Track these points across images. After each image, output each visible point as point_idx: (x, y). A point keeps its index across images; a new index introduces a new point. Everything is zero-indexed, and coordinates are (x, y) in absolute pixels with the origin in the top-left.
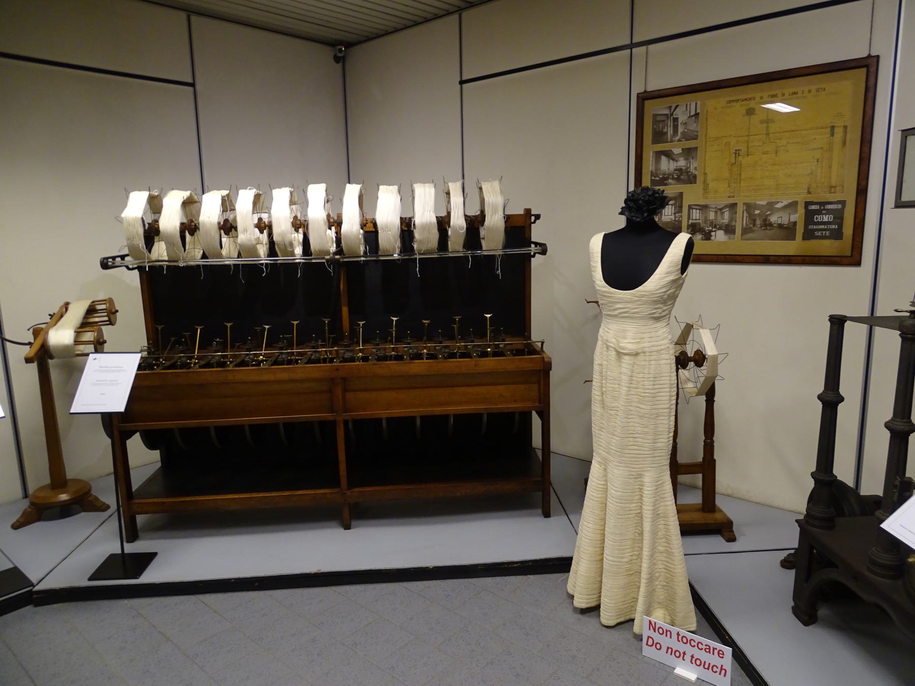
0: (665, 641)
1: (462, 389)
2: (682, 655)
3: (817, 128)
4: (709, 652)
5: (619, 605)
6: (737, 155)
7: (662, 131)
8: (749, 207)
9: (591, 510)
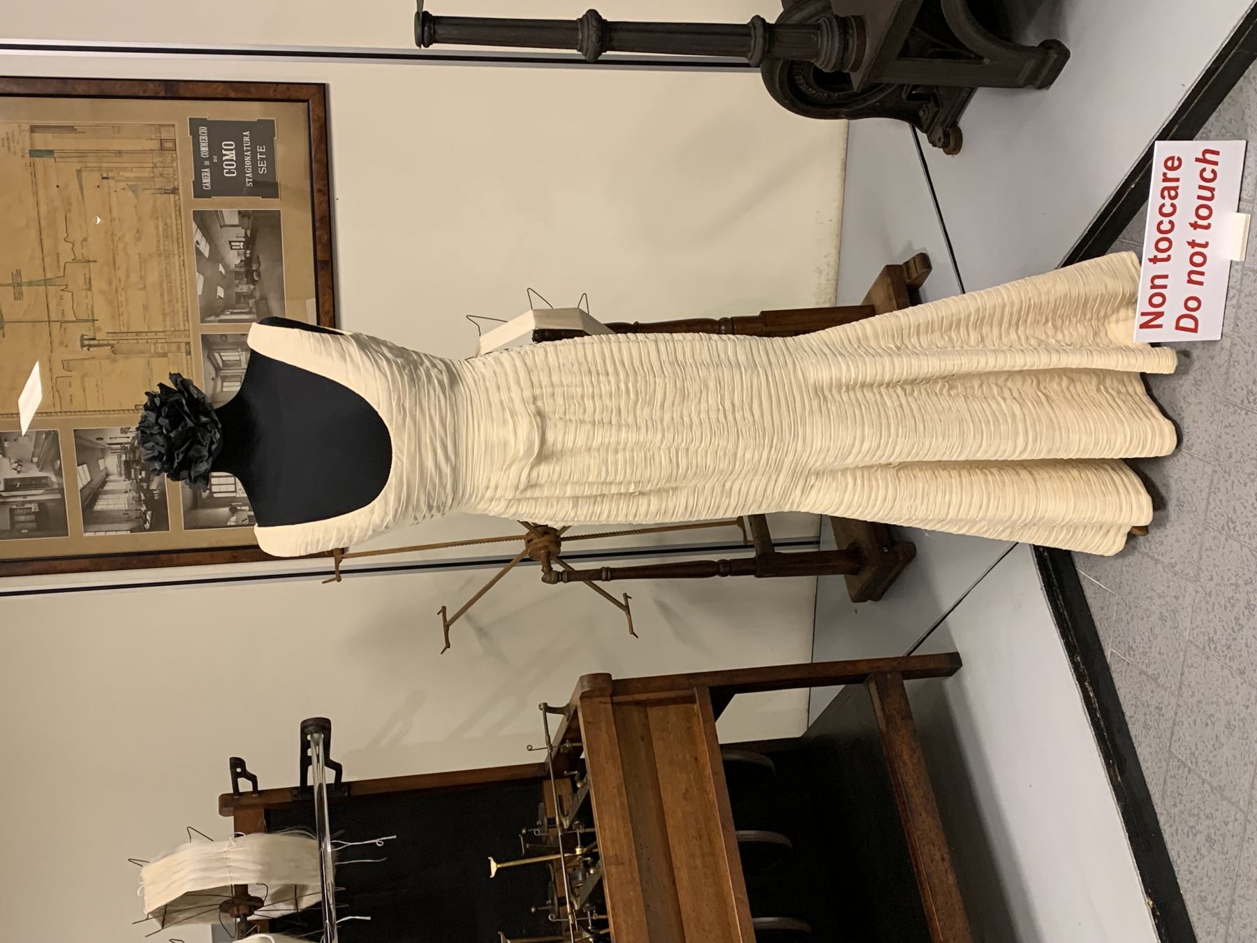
0: (1177, 291)
1: (684, 898)
2: (1197, 249)
3: (35, 184)
4: (1175, 189)
5: (1124, 416)
6: (92, 342)
7: (35, 513)
8: (210, 310)
9: (919, 501)
